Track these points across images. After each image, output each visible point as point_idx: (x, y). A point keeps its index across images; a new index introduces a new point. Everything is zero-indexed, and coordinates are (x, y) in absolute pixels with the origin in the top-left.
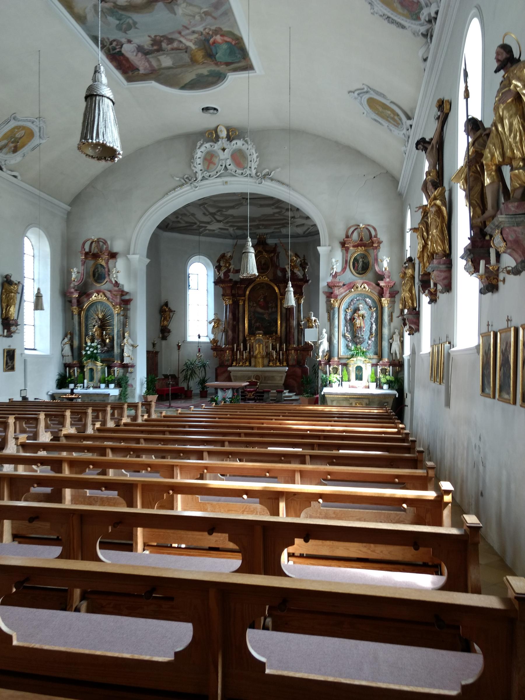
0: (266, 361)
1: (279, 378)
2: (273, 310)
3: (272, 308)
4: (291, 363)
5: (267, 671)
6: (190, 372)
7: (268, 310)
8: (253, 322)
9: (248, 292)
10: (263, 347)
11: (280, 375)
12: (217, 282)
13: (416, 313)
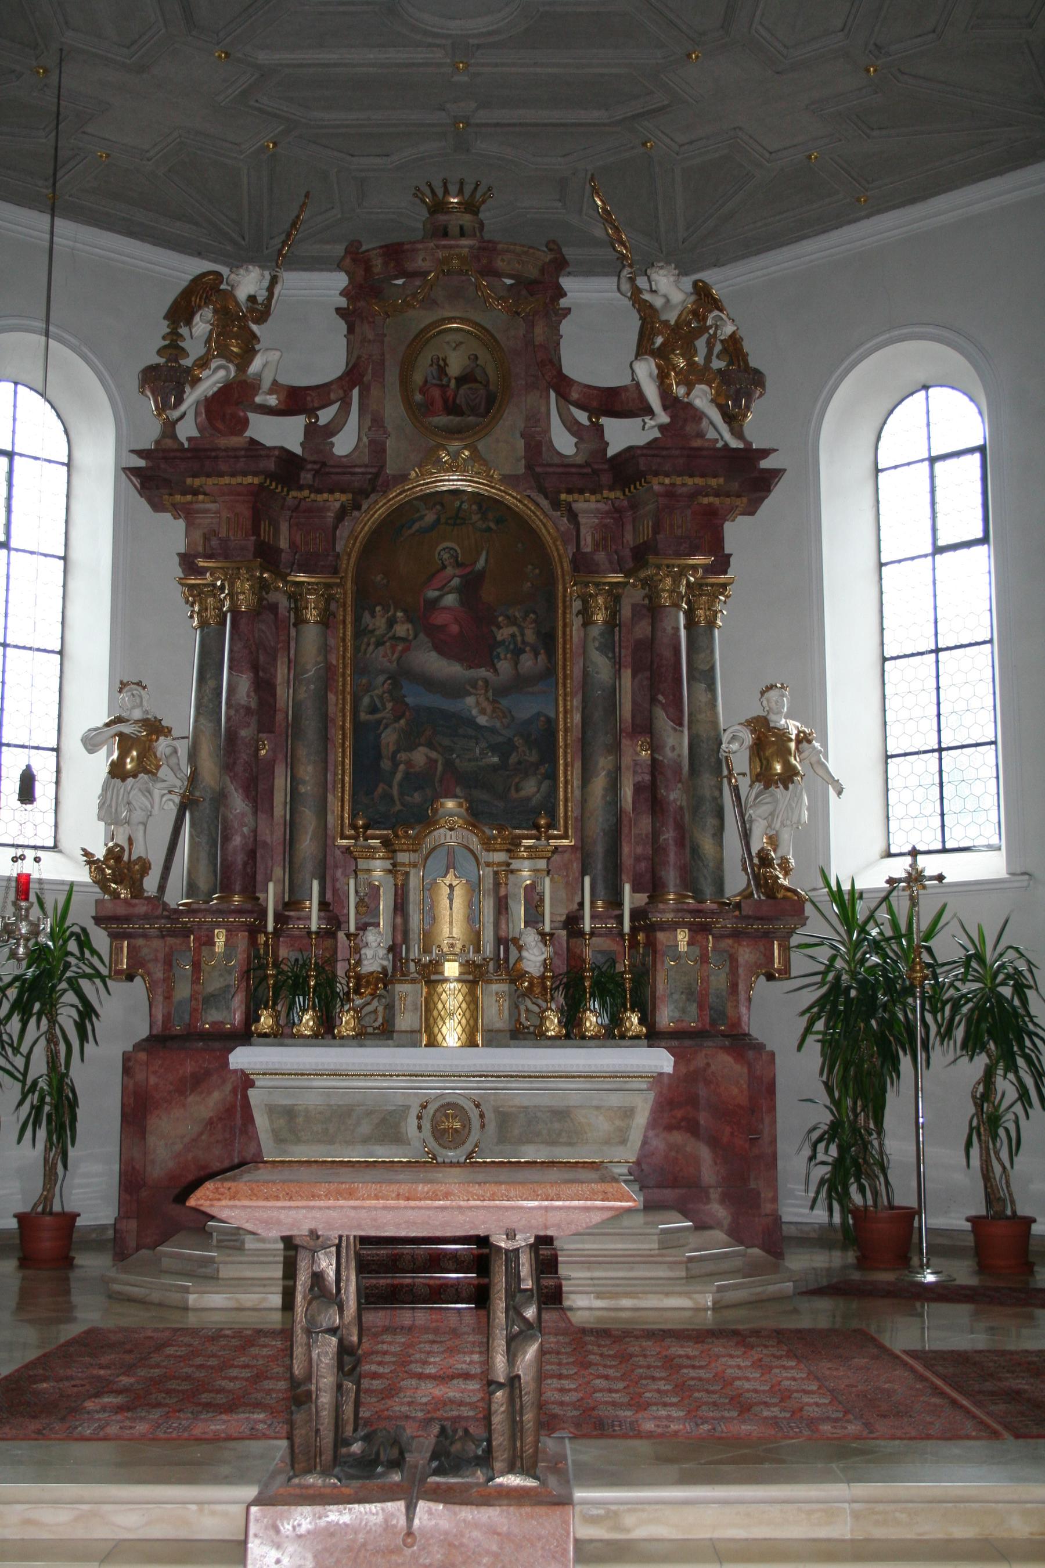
0: (495, 1000)
1: (602, 1125)
3: (517, 652)
6: (974, 964)
11: (615, 1100)
12: (156, 476)
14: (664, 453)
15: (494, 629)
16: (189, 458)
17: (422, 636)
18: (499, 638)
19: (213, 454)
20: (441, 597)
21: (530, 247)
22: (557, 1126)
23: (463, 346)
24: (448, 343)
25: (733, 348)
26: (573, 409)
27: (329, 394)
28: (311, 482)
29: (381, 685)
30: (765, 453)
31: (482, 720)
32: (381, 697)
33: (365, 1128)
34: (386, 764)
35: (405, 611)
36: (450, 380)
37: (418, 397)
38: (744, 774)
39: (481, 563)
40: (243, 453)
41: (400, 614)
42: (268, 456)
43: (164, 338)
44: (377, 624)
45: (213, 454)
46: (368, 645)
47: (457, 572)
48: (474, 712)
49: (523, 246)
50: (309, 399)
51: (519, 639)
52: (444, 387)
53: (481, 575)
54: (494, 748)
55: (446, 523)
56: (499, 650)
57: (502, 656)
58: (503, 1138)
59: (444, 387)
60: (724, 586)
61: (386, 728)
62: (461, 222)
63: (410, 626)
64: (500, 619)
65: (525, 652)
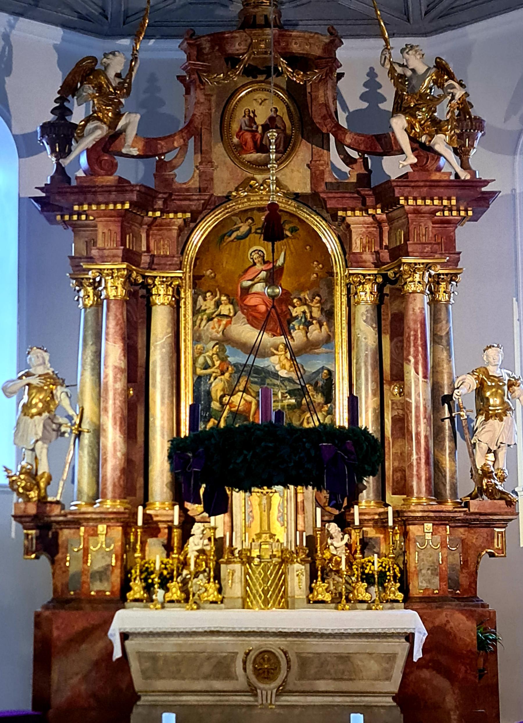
2: (316, 332)
3: (307, 324)
4: (418, 586)
5: (49, 182)
7: (286, 332)
8: (217, 387)
9: (197, 238)
10: (281, 506)
13: (442, 561)
14: (413, 184)
15: (290, 307)
16: (77, 192)
17: (239, 313)
18: (294, 314)
19: (94, 190)
20: (253, 285)
21: (316, 33)
22: (341, 667)
23: (267, 101)
24: (255, 100)
25: (464, 107)
26: (346, 148)
27: (173, 143)
28: (162, 207)
29: (211, 349)
30: (486, 183)
31: (283, 373)
32: (211, 358)
33: (207, 669)
34: (215, 405)
35: (227, 295)
36: (257, 128)
37: (236, 140)
38: (472, 411)
39: (280, 262)
40: (114, 188)
41: (223, 298)
42: (132, 191)
43: (56, 101)
44: (208, 305)
45: (94, 190)
46: (202, 320)
47: (263, 267)
48: (277, 367)
49: (311, 33)
50: (159, 146)
51: (308, 315)
52: (254, 133)
53: (281, 268)
54: (291, 393)
55: (256, 233)
56: (293, 323)
57: (296, 327)
58: (302, 676)
59: (254, 133)
60: (456, 275)
61: (215, 378)
62: (265, 13)
63: (231, 307)
64: (295, 301)
65: (313, 324)
